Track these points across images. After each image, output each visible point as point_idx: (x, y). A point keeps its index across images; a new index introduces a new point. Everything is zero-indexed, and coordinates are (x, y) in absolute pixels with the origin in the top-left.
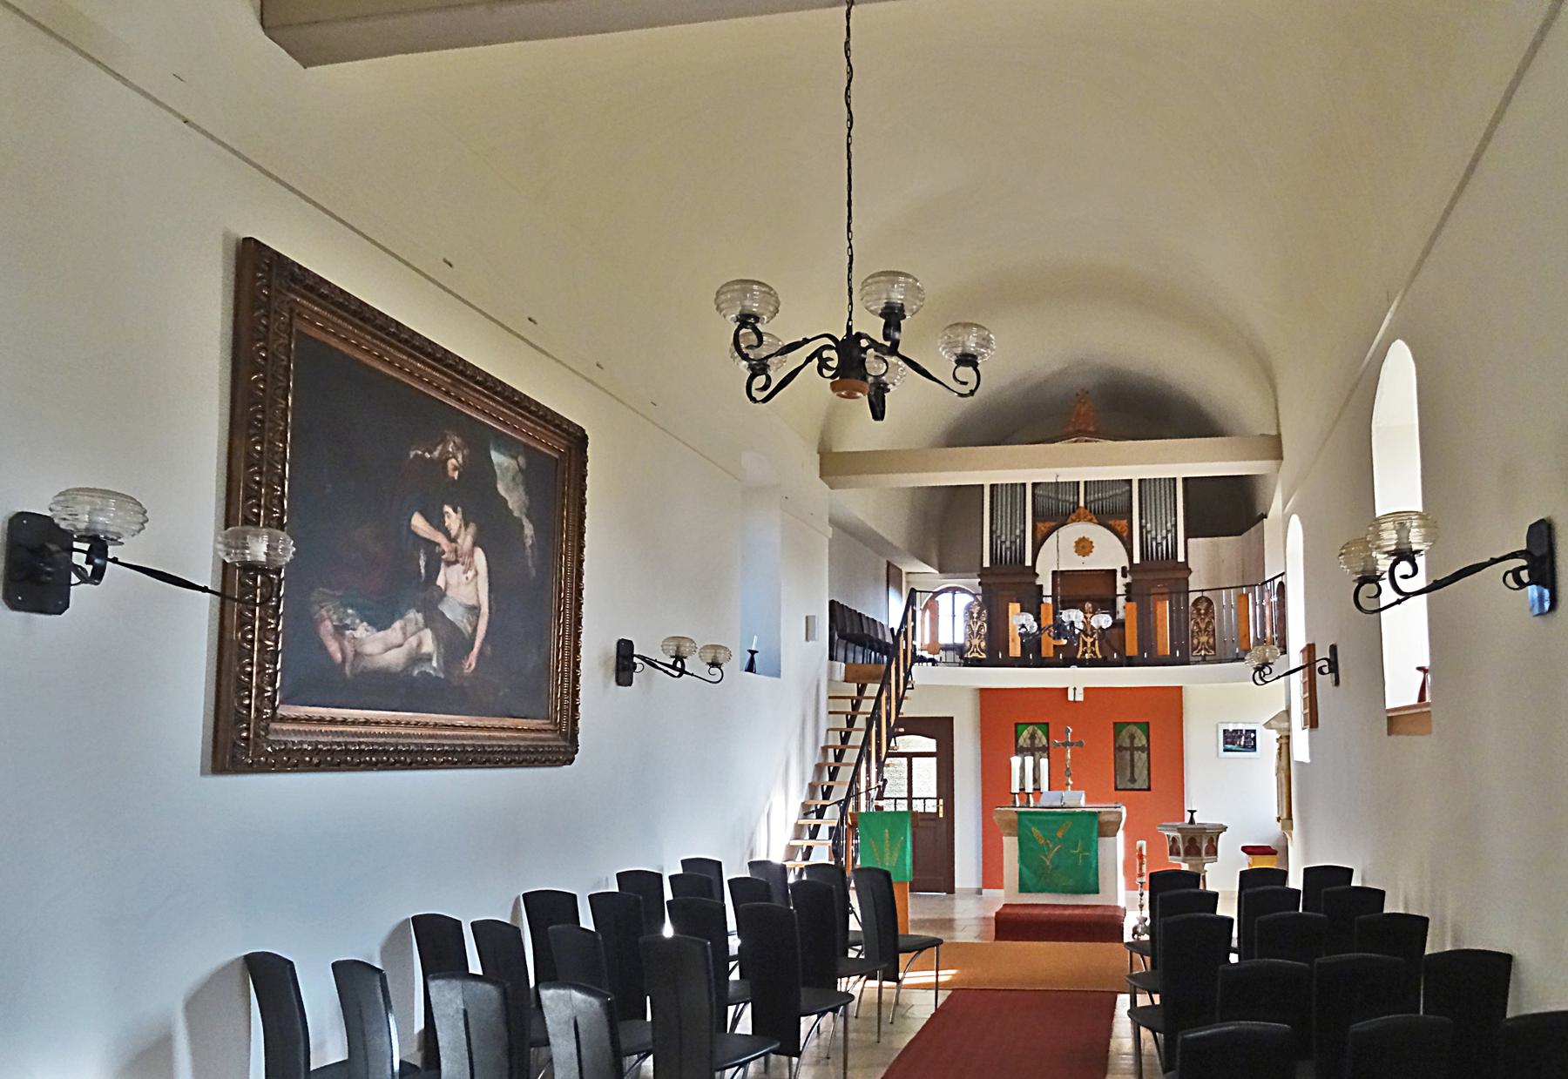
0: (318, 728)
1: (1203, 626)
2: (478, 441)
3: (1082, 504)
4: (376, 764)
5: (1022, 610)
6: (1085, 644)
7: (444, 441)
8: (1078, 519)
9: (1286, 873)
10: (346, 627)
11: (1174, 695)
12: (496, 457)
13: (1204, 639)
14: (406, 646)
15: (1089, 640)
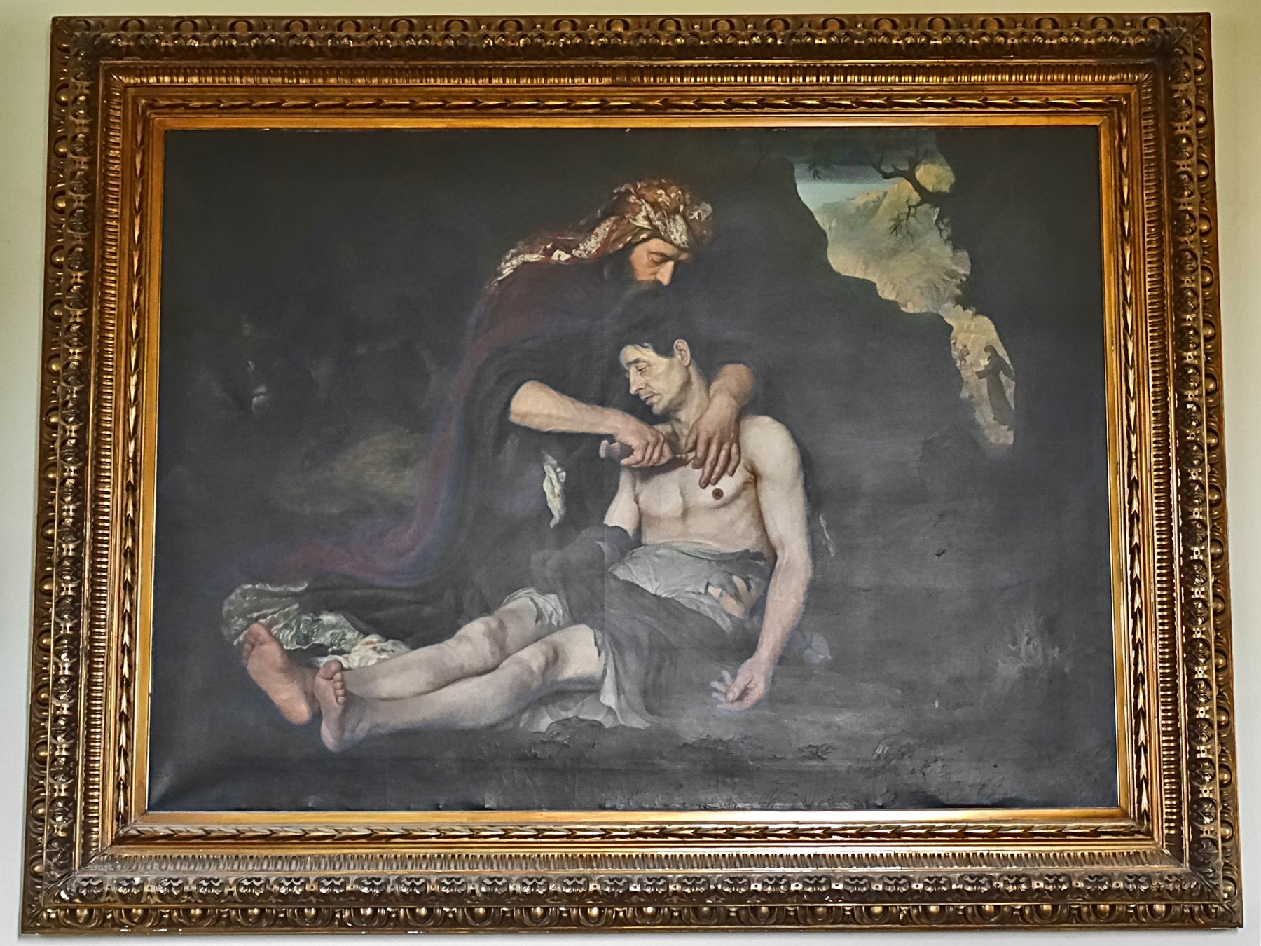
0: (856, 850)
2: (747, 174)
4: (852, 919)
5: (964, 309)
7: (618, 208)
10: (322, 650)
12: (814, 193)
14: (509, 669)
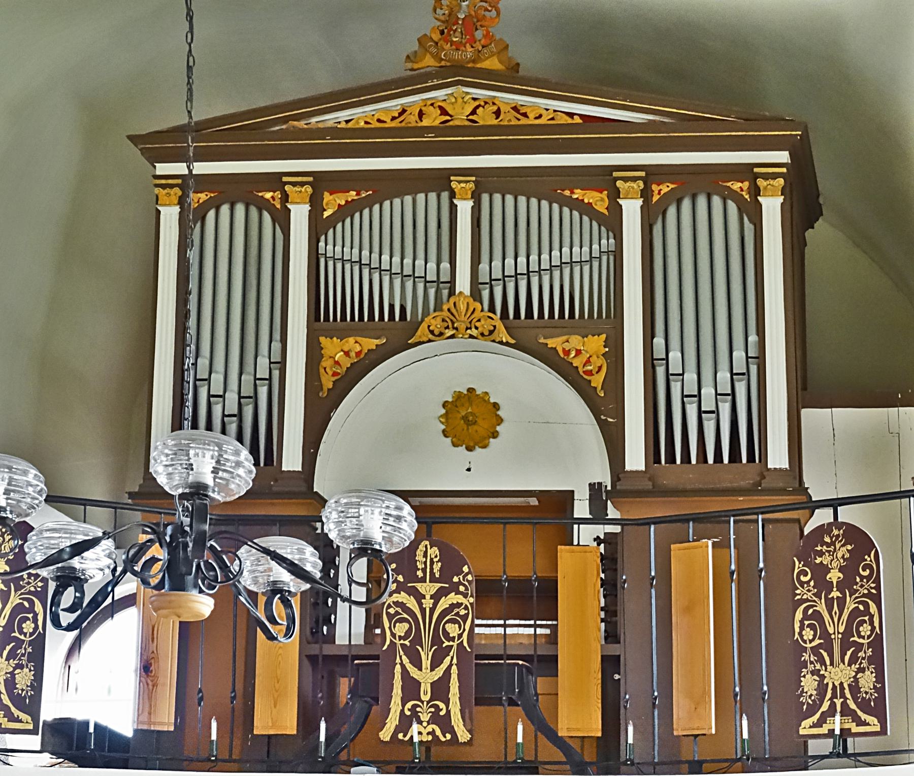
1: (836, 628)
3: (463, 284)
6: (411, 688)
8: (450, 329)
9: (555, 658)
11: (37, 734)
13: (839, 674)
15: (426, 677)
